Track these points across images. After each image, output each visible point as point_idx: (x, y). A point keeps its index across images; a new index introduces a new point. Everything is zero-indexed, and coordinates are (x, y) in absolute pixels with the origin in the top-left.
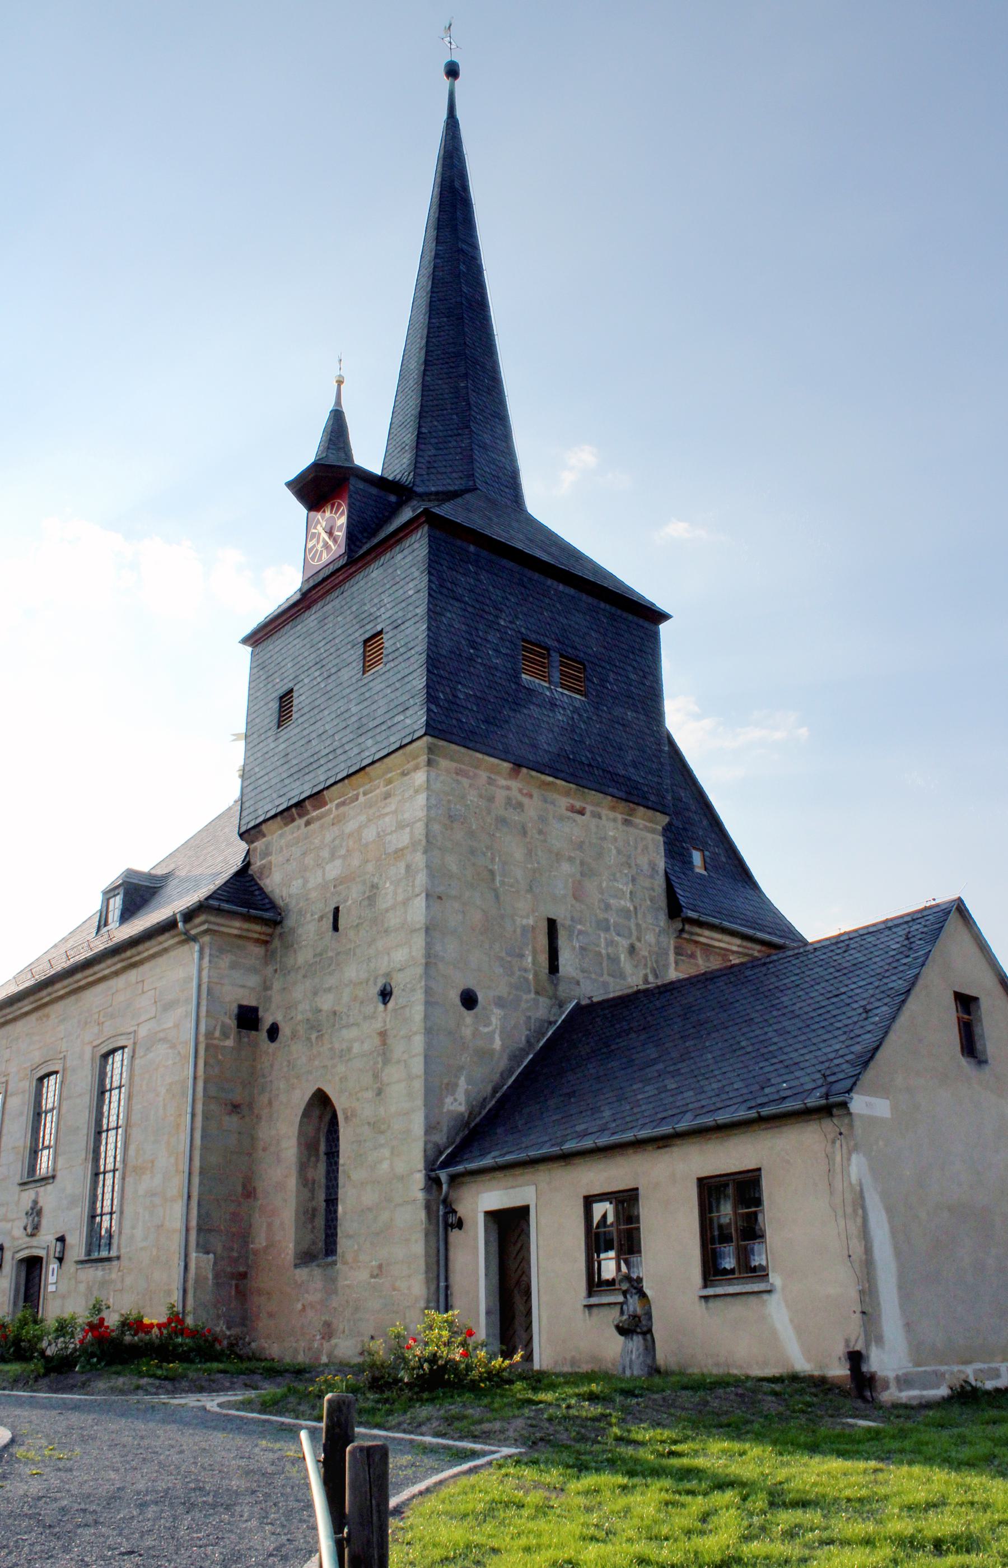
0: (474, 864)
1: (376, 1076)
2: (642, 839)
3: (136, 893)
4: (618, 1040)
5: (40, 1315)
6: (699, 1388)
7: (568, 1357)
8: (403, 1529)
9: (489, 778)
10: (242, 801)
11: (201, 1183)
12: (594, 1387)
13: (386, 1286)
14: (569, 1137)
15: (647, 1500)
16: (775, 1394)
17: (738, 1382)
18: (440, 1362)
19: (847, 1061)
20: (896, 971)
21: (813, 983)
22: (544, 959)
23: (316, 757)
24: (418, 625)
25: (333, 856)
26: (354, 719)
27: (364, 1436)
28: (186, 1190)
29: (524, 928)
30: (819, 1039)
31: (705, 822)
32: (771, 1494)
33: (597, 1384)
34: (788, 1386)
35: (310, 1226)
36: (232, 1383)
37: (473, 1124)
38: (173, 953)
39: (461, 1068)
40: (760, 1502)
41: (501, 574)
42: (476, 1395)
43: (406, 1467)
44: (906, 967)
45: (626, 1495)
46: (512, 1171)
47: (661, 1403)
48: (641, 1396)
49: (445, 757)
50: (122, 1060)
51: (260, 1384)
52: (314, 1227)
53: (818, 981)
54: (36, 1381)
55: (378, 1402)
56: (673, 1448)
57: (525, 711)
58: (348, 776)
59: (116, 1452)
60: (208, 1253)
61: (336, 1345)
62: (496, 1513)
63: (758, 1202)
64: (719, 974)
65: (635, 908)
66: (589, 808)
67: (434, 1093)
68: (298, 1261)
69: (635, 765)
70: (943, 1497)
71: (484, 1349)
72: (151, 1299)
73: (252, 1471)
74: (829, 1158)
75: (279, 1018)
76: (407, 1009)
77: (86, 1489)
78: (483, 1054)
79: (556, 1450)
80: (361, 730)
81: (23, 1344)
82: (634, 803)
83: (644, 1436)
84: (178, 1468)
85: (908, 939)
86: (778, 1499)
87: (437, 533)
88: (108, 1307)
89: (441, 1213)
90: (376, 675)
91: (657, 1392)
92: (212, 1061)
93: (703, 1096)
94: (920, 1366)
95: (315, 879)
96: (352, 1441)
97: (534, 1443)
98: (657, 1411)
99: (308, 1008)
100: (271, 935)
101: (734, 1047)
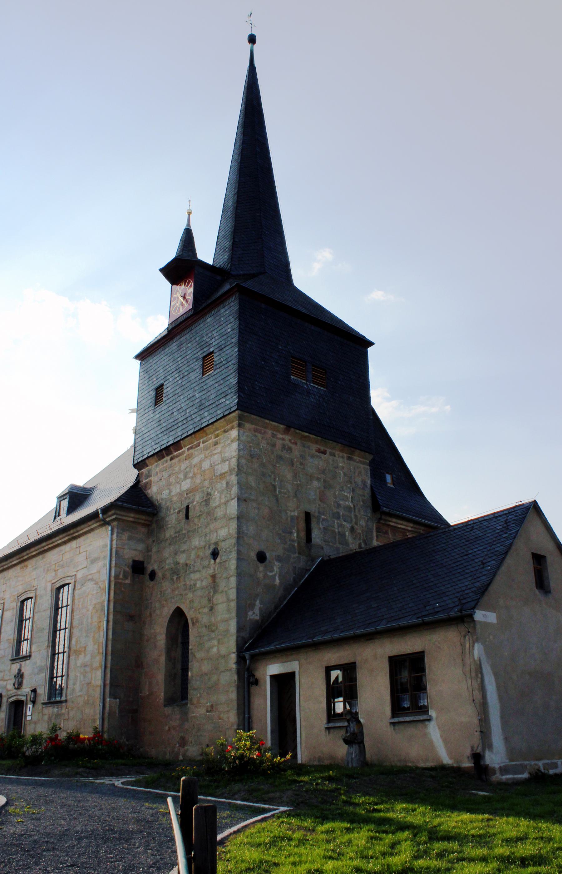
0: (264, 482)
1: (210, 600)
2: (358, 468)
3: (76, 497)
8: (224, 852)
9: (273, 433)
13: (215, 714)
16: (432, 777)
19: (472, 592)
20: (500, 541)
21: (453, 548)
22: (303, 534)
23: (176, 422)
24: (233, 349)
25: (186, 477)
27: (203, 801)
28: (104, 663)
29: (292, 518)
33: (333, 772)
38: (96, 531)
39: (257, 595)
43: (226, 818)
48: (358, 778)
49: (248, 422)
56: (375, 807)
57: (293, 397)
60: (116, 699)
61: (187, 750)
62: (276, 844)
63: (423, 670)
65: (354, 506)
66: (328, 451)
67: (242, 609)
72: (84, 724)
73: (141, 820)
74: (463, 645)
76: (227, 563)
80: (201, 407)
81: (13, 749)
82: (353, 447)
83: (359, 801)
84: (99, 818)
85: (506, 523)
86: (434, 835)
89: (246, 676)
90: (210, 376)
94: (513, 761)
95: (176, 490)
96: (197, 804)
99: (172, 562)
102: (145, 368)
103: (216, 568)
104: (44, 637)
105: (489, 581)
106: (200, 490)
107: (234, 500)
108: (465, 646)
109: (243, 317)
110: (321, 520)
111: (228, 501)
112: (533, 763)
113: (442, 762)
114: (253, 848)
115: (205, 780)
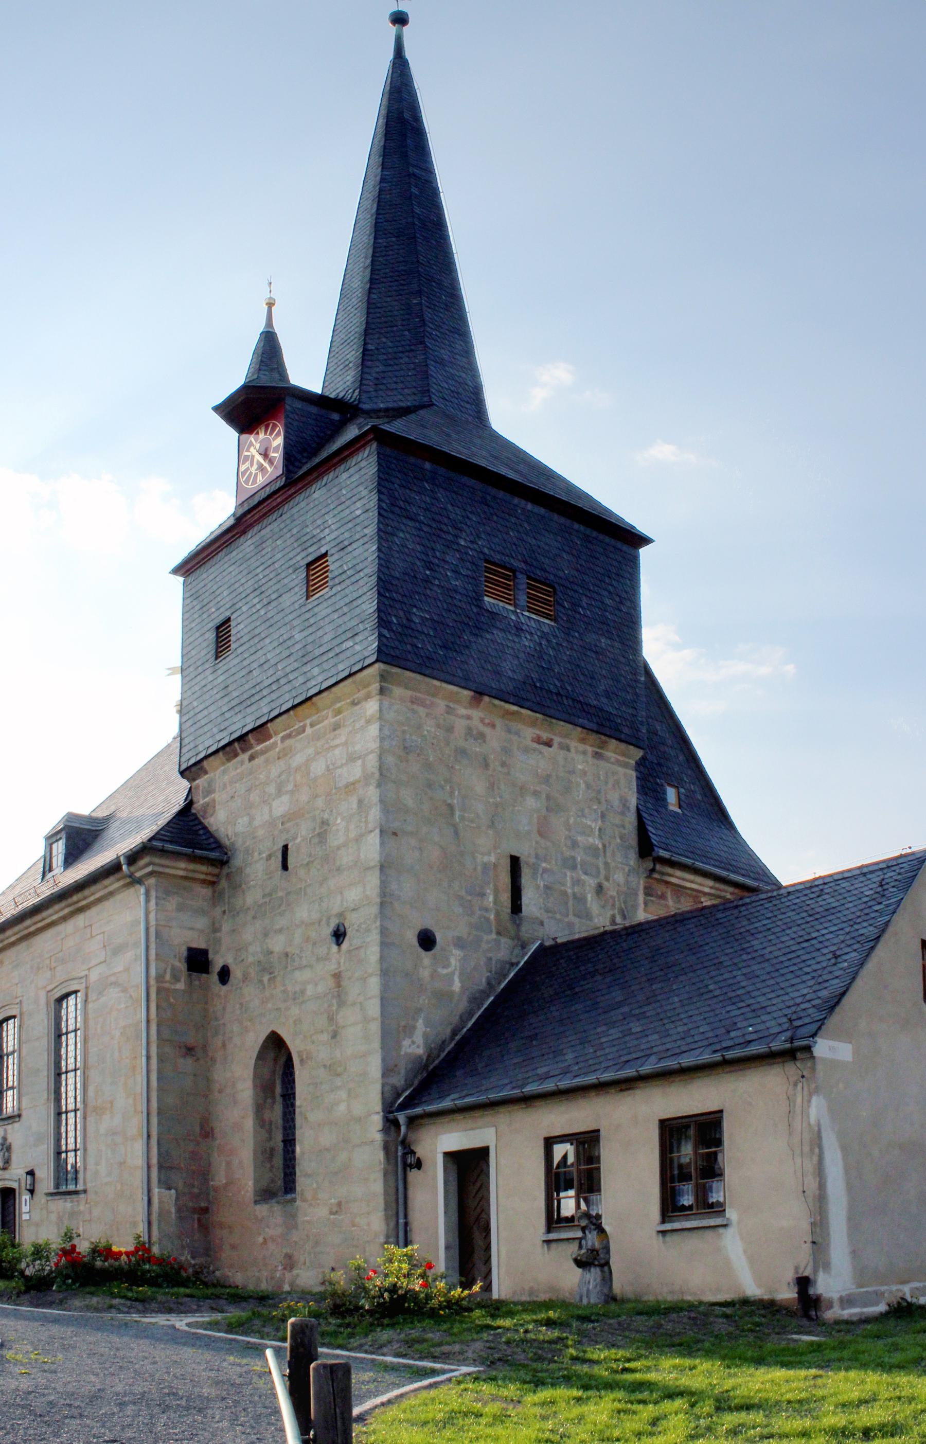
0: (431, 799)
2: (614, 773)
3: (78, 837)
4: (582, 983)
5: (17, 1240)
6: (653, 1313)
7: (527, 1288)
8: (366, 1433)
9: (448, 706)
10: (181, 737)
11: (159, 1123)
12: (551, 1313)
13: (345, 1219)
14: (530, 1080)
15: (600, 1410)
16: (726, 1316)
17: (691, 1307)
18: (400, 1292)
19: (814, 1006)
20: (868, 917)
21: (784, 927)
23: (258, 688)
24: (366, 546)
25: (280, 792)
26: (298, 646)
27: (327, 1355)
28: (145, 1130)
29: (485, 866)
30: (787, 984)
31: (681, 758)
32: (718, 1400)
33: (555, 1312)
34: (739, 1309)
35: (268, 1165)
36: (199, 1306)
37: (431, 1067)
38: (118, 897)
39: (419, 1010)
40: (707, 1407)
41: (461, 492)
42: (435, 1322)
43: (368, 1382)
44: (878, 914)
45: (580, 1405)
46: (473, 1114)
47: (616, 1327)
48: (597, 1321)
49: (399, 685)
50: (76, 1004)
51: (225, 1308)
52: (272, 1166)
53: (789, 925)
54: (18, 1296)
55: (340, 1326)
56: (627, 1365)
57: (488, 636)
58: (294, 707)
59: (95, 1360)
60: (169, 1189)
61: (298, 1275)
62: (455, 1421)
63: (719, 1142)
64: (689, 915)
65: (604, 846)
66: (557, 740)
67: (390, 1037)
68: (258, 1198)
69: (607, 694)
70: (874, 1394)
71: (444, 1281)
72: (118, 1229)
73: (221, 1381)
74: (790, 1099)
75: (230, 960)
76: (362, 951)
77: (70, 1388)
78: (442, 996)
79: (514, 1368)
80: (306, 658)
81: (4, 1264)
82: (605, 735)
83: (599, 1356)
84: (152, 1375)
85: (881, 886)
86: (723, 1404)
87: (388, 451)
88: (79, 1236)
89: (400, 1154)
90: (321, 599)
91: (613, 1318)
92: (164, 1004)
93: (668, 1039)
94: (862, 1287)
95: (261, 816)
96: (316, 1359)
97: (492, 1362)
98: (612, 1334)
99: (259, 949)
100: (217, 876)
101: (702, 991)
102: (194, 591)
103: (342, 961)
104: (42, 1082)
105: (844, 988)
106: (307, 816)
107: (373, 834)
108: (795, 1102)
109: (384, 484)
110: (541, 871)
111: (361, 835)
112: (894, 1288)
113: (744, 1292)
114: (415, 1428)
115: (330, 1323)
